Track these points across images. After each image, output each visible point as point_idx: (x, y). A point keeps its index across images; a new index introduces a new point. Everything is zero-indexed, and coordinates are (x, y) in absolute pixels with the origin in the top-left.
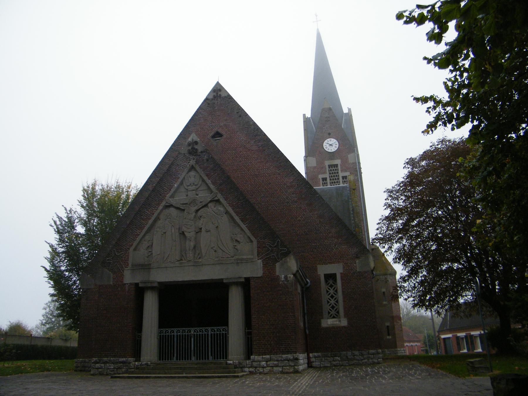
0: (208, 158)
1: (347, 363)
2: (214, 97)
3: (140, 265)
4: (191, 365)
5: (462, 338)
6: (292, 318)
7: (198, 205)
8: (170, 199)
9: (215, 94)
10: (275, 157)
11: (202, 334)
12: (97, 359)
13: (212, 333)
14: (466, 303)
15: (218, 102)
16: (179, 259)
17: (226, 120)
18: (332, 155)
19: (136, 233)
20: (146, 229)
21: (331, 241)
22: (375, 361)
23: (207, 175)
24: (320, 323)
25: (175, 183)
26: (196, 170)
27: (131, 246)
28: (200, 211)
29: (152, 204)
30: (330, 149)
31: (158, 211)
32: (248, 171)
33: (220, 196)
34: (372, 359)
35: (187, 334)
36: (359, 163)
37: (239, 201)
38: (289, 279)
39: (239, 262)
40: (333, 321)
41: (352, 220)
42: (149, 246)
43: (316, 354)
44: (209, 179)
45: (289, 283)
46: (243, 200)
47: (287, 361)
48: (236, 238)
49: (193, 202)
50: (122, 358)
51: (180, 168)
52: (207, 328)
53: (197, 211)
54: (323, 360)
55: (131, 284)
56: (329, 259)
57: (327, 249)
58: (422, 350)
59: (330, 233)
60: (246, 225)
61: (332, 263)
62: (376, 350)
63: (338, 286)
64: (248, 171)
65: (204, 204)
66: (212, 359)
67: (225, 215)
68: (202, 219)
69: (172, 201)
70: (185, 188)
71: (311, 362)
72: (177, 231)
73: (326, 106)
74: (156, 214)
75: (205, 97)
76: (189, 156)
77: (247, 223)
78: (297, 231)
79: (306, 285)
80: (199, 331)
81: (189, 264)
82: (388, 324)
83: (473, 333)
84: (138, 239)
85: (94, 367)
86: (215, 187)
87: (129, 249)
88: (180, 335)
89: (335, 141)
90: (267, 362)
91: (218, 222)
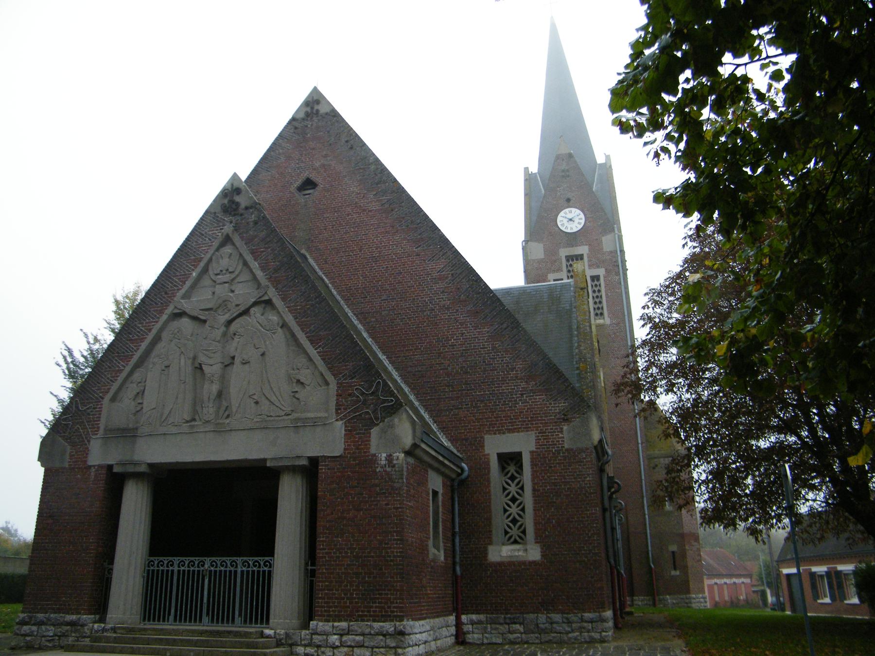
0: (256, 219)
1: (537, 638)
2: (307, 115)
3: (118, 429)
4: (190, 634)
5: (821, 576)
6: (397, 544)
7: (231, 312)
8: (182, 301)
9: (308, 109)
10: (412, 222)
11: (225, 571)
12: (26, 615)
13: (244, 569)
14: (812, 513)
15: (312, 125)
16: (188, 419)
17: (326, 156)
18: (573, 238)
19: (118, 366)
20: (135, 360)
21: (514, 386)
22: (595, 637)
23: (253, 253)
24: (485, 553)
25: (193, 270)
26: (233, 244)
27: (107, 392)
28: (234, 323)
29: (150, 311)
30: (569, 226)
31: (158, 326)
32: (361, 251)
33: (272, 294)
34: (588, 631)
35: (187, 569)
36: (622, 252)
37: (308, 301)
38: (395, 462)
39: (299, 425)
40: (512, 550)
41: (574, 348)
42: (138, 393)
43: (474, 617)
44: (255, 260)
45: (395, 471)
46: (315, 299)
47: (381, 637)
48: (298, 377)
49: (224, 304)
50: (73, 614)
51: (205, 240)
52: (224, 559)
53: (229, 322)
54: (489, 630)
55: (99, 466)
56: (509, 423)
57: (505, 401)
58: (754, 592)
59: (512, 369)
60: (318, 350)
61: (513, 432)
62: (598, 614)
63: (525, 477)
64: (361, 251)
65: (242, 308)
66: (241, 623)
67: (280, 330)
68: (236, 339)
69: (185, 305)
70: (211, 279)
71: (464, 634)
72: (189, 362)
73: (564, 150)
74: (154, 331)
75: (290, 117)
76: (223, 217)
77: (320, 346)
78: (449, 366)
79: (459, 475)
80: (219, 565)
81: (207, 429)
82: (673, 548)
83: (840, 568)
84: (120, 380)
85: (18, 632)
86: (266, 275)
87: (103, 398)
88: (184, 571)
89: (578, 211)
90: (341, 635)
91: (266, 345)
